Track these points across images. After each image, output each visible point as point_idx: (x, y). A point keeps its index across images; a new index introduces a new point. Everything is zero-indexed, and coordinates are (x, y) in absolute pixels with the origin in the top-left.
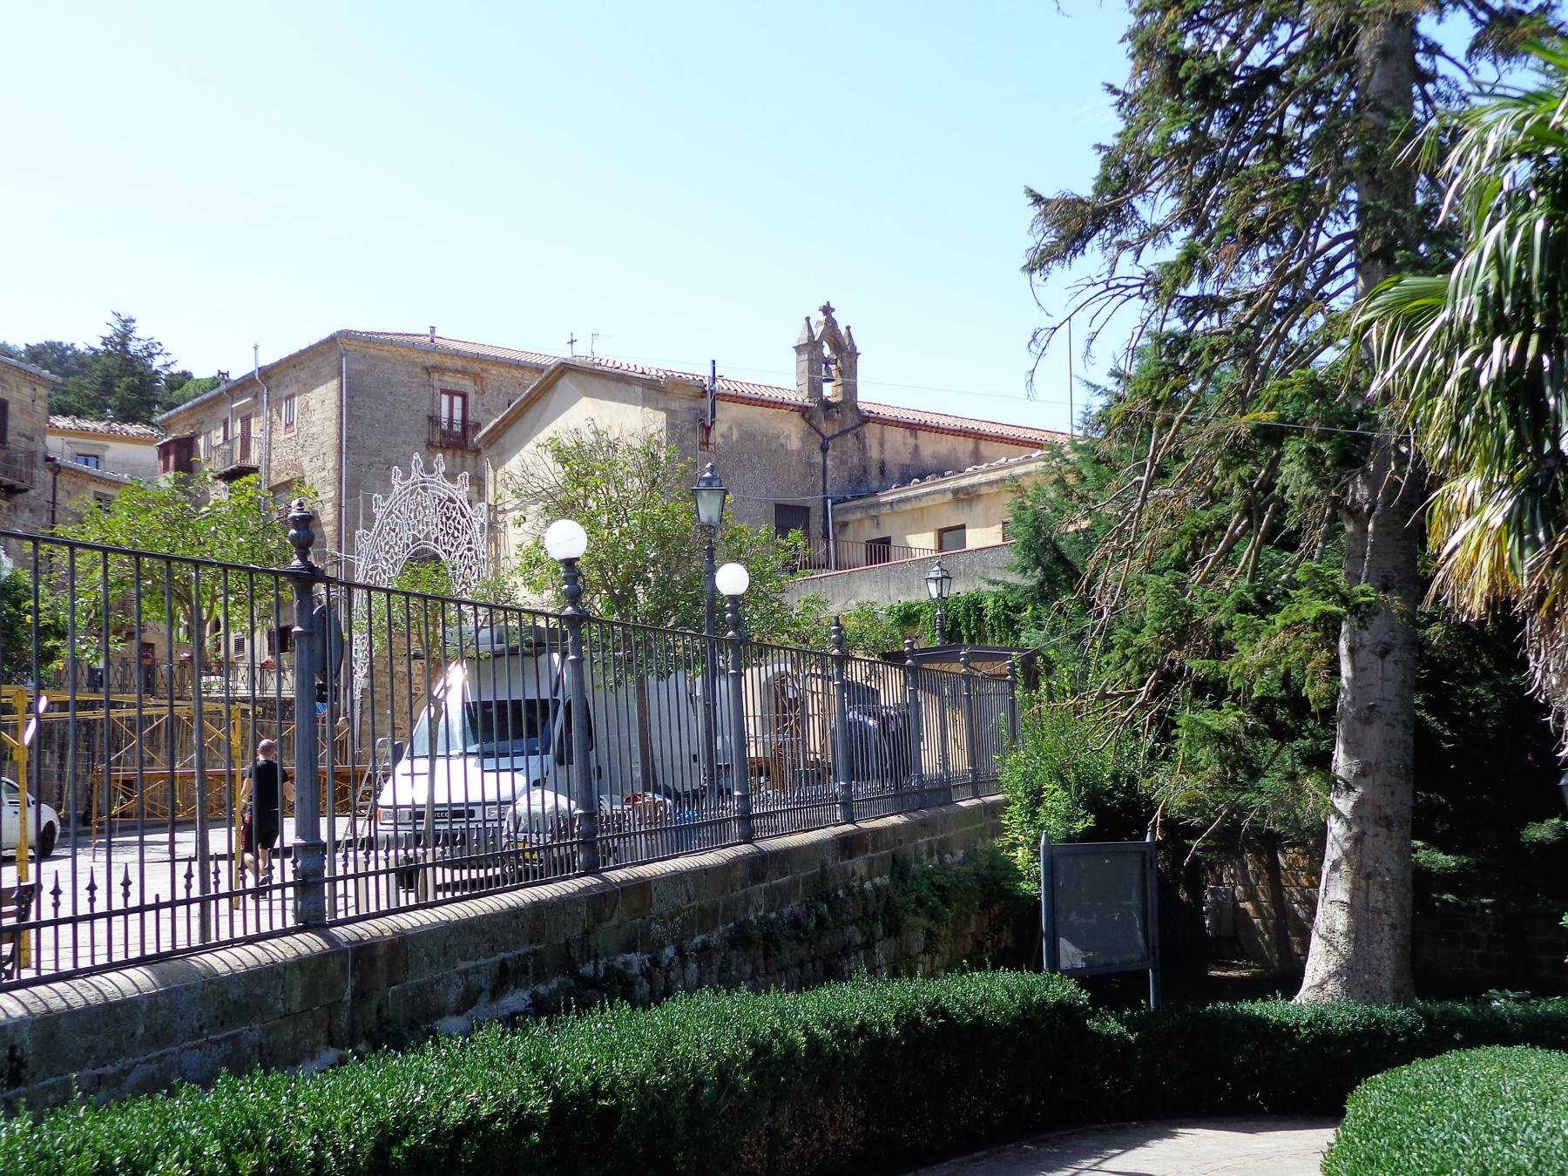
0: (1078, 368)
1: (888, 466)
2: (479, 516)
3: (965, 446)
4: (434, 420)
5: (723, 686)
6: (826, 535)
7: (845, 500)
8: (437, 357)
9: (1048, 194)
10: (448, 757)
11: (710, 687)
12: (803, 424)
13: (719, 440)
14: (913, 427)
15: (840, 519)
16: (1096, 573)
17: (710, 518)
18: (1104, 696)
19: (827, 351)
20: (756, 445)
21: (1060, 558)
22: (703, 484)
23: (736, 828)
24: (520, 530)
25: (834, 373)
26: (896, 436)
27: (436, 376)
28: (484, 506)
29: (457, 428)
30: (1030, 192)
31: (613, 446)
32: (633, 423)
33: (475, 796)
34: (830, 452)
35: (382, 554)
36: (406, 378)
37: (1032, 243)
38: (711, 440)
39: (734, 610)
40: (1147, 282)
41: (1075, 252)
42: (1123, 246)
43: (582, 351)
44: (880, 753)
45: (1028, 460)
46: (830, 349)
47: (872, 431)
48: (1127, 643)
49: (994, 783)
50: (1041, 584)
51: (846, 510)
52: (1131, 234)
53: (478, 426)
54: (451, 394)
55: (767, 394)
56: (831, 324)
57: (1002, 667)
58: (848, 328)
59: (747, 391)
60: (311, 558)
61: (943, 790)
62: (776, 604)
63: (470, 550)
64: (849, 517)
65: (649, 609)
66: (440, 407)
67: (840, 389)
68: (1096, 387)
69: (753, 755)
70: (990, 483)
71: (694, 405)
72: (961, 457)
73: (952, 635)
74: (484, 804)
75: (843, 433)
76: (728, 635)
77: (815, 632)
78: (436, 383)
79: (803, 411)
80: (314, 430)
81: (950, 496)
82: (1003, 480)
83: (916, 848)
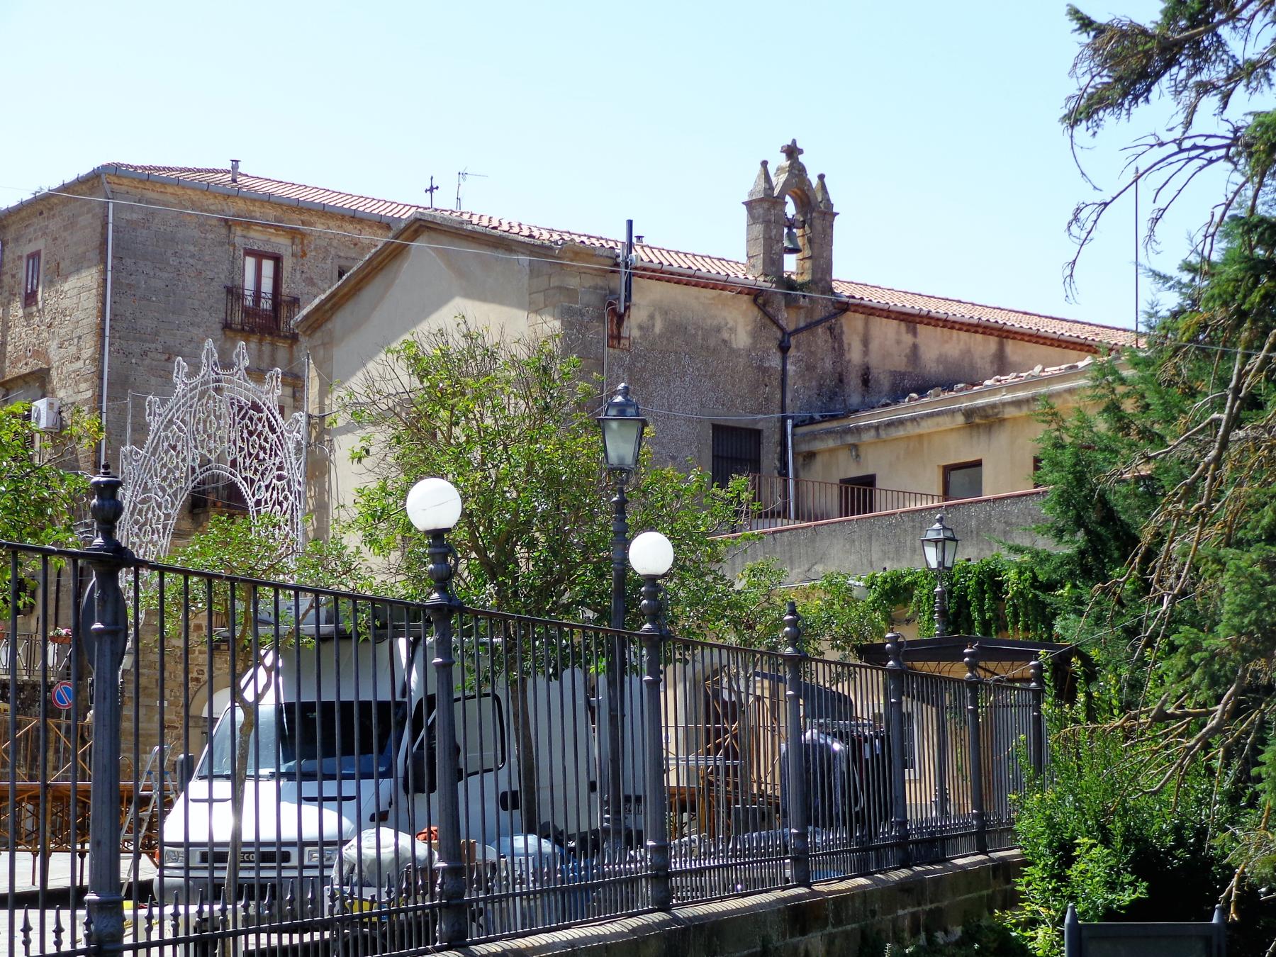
0: (1142, 260)
1: (874, 372)
2: (293, 431)
3: (984, 347)
4: (234, 292)
5: (635, 685)
6: (783, 472)
7: (812, 421)
8: (241, 204)
9: (1100, 18)
10: (257, 778)
11: (616, 684)
12: (755, 312)
13: (636, 333)
14: (911, 320)
15: (805, 448)
16: (1159, 538)
17: (621, 459)
18: (1162, 717)
19: (791, 210)
20: (690, 343)
21: (1109, 516)
22: (613, 412)
23: (646, 889)
24: (356, 467)
25: (800, 242)
26: (887, 331)
27: (238, 231)
28: (301, 416)
29: (266, 305)
30: (1075, 14)
31: (491, 355)
32: (513, 328)
33: (289, 834)
34: (792, 352)
35: (157, 481)
36: (196, 233)
37: (1072, 88)
38: (625, 332)
39: (652, 596)
40: (1235, 140)
41: (1136, 98)
42: (1204, 88)
43: (444, 202)
44: (851, 792)
45: (1073, 371)
46: (795, 209)
47: (852, 325)
48: (1195, 646)
49: (1007, 833)
50: (1082, 553)
51: (814, 436)
52: (1216, 72)
53: (295, 302)
54: (259, 256)
55: (704, 268)
56: (797, 171)
57: (1029, 668)
58: (821, 177)
59: (677, 263)
60: (121, 536)
61: (933, 846)
62: (709, 578)
63: (280, 478)
64: (818, 446)
65: (537, 594)
66: (241, 276)
67: (808, 264)
68: (1165, 279)
69: (673, 783)
70: (1018, 403)
71: (597, 286)
72: (979, 363)
73: (956, 616)
74: (302, 844)
75: (810, 326)
76: (637, 624)
77: (763, 613)
78: (238, 241)
79: (756, 295)
80: (66, 303)
81: (960, 419)
82: (1034, 399)
83: (894, 921)
